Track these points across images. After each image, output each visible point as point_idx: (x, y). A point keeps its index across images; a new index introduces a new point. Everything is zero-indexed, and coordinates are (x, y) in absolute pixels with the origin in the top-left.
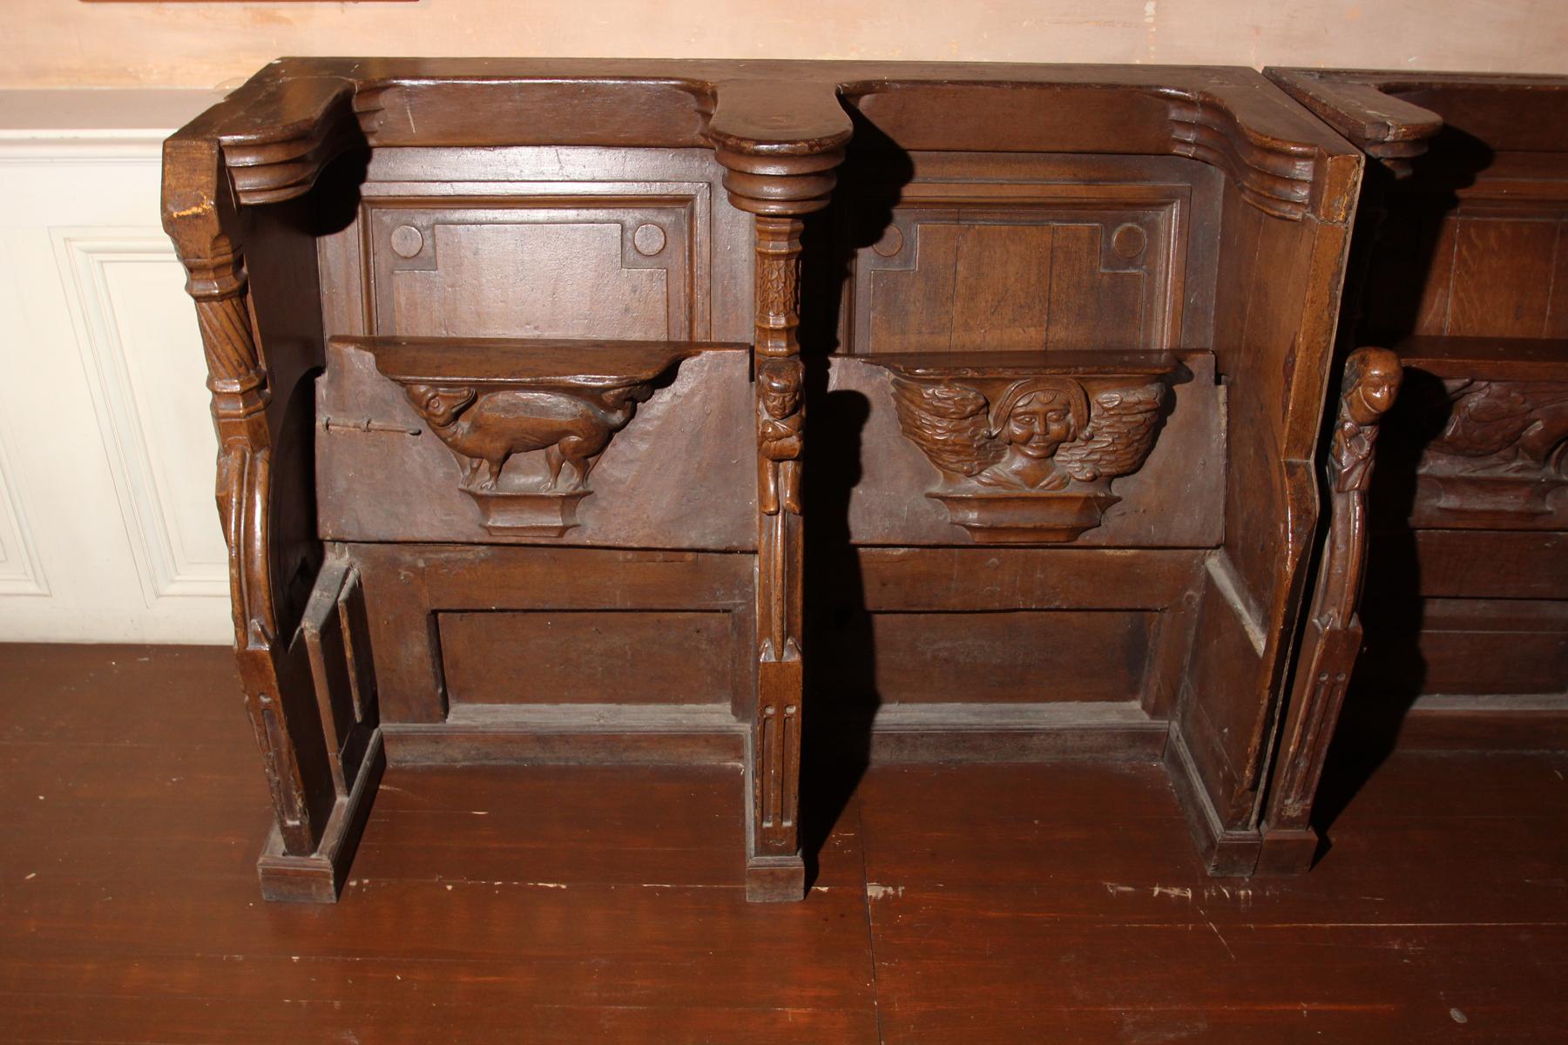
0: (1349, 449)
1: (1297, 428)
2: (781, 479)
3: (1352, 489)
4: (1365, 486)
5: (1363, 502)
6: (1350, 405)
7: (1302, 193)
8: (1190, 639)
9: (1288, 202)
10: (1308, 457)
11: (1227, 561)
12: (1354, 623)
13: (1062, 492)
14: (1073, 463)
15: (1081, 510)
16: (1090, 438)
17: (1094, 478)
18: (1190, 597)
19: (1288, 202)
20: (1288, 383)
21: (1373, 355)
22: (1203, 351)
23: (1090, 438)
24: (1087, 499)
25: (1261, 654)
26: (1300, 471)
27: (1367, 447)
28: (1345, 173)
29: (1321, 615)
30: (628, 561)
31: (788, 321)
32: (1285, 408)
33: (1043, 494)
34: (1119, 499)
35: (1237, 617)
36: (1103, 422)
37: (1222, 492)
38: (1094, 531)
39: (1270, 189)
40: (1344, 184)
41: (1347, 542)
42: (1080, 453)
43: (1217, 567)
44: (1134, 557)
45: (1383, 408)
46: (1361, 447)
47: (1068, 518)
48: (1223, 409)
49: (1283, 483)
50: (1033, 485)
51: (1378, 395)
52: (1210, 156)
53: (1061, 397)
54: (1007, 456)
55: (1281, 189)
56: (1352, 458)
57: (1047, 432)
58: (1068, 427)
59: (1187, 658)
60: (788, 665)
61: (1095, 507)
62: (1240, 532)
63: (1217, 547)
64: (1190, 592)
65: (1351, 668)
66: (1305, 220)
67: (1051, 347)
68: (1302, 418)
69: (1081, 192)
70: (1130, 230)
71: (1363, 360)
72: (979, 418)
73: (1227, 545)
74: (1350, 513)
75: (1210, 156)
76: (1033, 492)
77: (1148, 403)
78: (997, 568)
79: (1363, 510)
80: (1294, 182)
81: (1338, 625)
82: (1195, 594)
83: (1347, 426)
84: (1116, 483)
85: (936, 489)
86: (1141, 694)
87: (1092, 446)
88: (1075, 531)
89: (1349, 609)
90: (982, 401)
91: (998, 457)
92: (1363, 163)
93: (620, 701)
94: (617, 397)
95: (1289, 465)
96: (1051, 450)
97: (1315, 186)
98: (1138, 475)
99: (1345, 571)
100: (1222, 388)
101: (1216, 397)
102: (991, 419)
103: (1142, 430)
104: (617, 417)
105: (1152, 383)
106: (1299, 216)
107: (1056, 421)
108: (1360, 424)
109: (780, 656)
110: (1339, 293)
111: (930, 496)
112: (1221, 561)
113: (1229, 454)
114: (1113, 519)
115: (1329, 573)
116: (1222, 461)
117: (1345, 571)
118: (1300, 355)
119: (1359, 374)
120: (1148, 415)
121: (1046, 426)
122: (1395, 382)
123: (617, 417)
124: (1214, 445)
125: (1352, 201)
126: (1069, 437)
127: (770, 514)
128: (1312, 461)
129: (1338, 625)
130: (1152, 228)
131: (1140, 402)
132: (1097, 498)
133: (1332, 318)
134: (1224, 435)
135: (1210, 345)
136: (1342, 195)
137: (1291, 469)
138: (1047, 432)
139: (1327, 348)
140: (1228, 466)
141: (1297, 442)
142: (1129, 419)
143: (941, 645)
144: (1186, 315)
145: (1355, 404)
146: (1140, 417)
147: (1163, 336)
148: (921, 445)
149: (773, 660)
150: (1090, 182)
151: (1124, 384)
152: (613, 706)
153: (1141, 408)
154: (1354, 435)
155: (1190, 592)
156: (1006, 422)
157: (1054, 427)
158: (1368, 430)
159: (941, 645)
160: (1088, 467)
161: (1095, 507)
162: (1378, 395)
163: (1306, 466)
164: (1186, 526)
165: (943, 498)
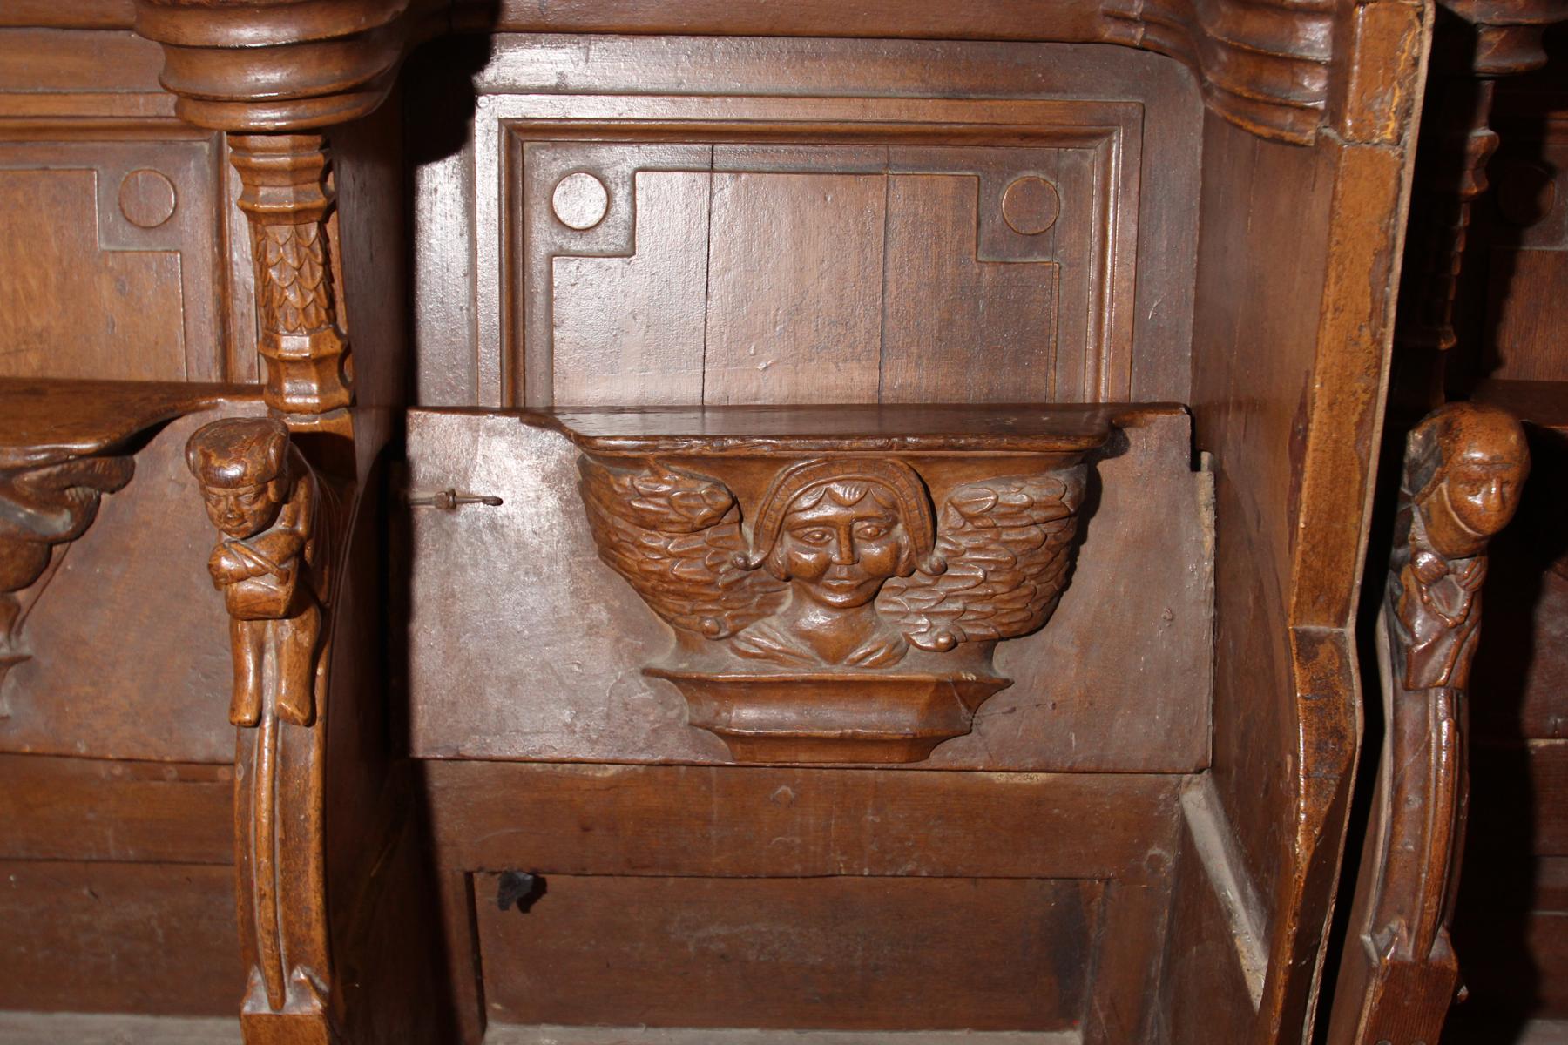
0: (1426, 604)
1: (1317, 564)
2: (270, 657)
3: (1432, 684)
4: (1459, 678)
5: (1454, 711)
6: (1427, 519)
7: (1315, 85)
8: (1161, 932)
9: (1286, 106)
10: (1341, 620)
11: (1216, 800)
12: (1440, 950)
13: (891, 673)
14: (918, 624)
15: (930, 705)
16: (940, 571)
17: (953, 645)
18: (1157, 860)
19: (1286, 106)
20: (1298, 473)
21: (1467, 419)
22: (1169, 407)
23: (940, 571)
24: (940, 685)
25: (1257, 1002)
26: (1324, 651)
27: (1462, 601)
28: (1391, 38)
29: (1377, 928)
30: (119, 779)
31: (315, 344)
32: (1293, 523)
33: (853, 674)
34: (1007, 683)
35: (1223, 916)
36: (964, 542)
37: (1207, 673)
38: (961, 741)
39: (1253, 83)
40: (1390, 62)
41: (1424, 791)
42: (927, 601)
43: (1199, 808)
44: (1046, 786)
45: (1489, 528)
46: (1450, 601)
47: (904, 719)
48: (1208, 517)
49: (1291, 675)
50: (835, 659)
51: (1478, 501)
52: (1167, 42)
53: (880, 493)
54: (788, 601)
55: (1272, 78)
56: (1436, 621)
57: (854, 558)
58: (897, 550)
59: (1157, 965)
60: (297, 1021)
61: (958, 700)
62: (1235, 751)
63: (1199, 771)
64: (1155, 851)
65: (1437, 1031)
66: (1322, 142)
67: (889, 397)
68: (1328, 546)
69: (932, 112)
70: (1031, 182)
71: (1448, 429)
72: (724, 532)
73: (1217, 768)
74: (1430, 729)
75: (1167, 42)
76: (837, 672)
77: (1045, 506)
78: (792, 803)
79: (1456, 728)
80: (1296, 64)
81: (1408, 953)
82: (1164, 854)
83: (1425, 559)
84: (1002, 653)
85: (660, 661)
86: (1083, 1020)
87: (943, 588)
88: (919, 746)
89: (1429, 920)
90: (723, 500)
91: (768, 605)
92: (1430, 19)
93: (158, 1010)
94: (40, 484)
95: (1302, 637)
96: (868, 589)
97: (1338, 72)
98: (1043, 636)
99: (1421, 849)
100: (1205, 478)
101: (1193, 493)
102: (748, 531)
103: (1042, 557)
104: (61, 522)
105: (1058, 467)
106: (1309, 136)
107: (872, 538)
108: (1445, 556)
109: (278, 1002)
110: (1393, 292)
111: (648, 672)
112: (1208, 797)
113: (1220, 598)
114: (995, 720)
115: (1390, 850)
116: (1207, 613)
117: (1421, 849)
118: (1317, 416)
119: (1442, 457)
120: (1051, 529)
121: (853, 548)
122: (1513, 474)
123: (61, 522)
124: (1190, 584)
125: (1409, 98)
126: (899, 567)
127: (242, 725)
128: (1350, 630)
129: (1408, 953)
130: (1075, 181)
131: (1031, 505)
132: (958, 683)
133: (1380, 344)
134: (1208, 565)
135: (1185, 397)
136: (1388, 84)
137: (1308, 645)
138: (854, 558)
139: (1370, 405)
140: (1217, 623)
141: (1319, 592)
142: (1014, 535)
143: (714, 930)
144: (1140, 340)
145: (1435, 514)
146: (1034, 532)
147: (1099, 382)
148: (629, 580)
149: (266, 1009)
150: (953, 95)
151: (1003, 469)
152: (146, 1020)
153: (1037, 515)
154: (1436, 578)
155: (1155, 851)
156: (776, 539)
157: (874, 551)
158: (1464, 566)
159: (714, 930)
160: (942, 623)
161: (958, 700)
162: (1478, 501)
163: (1338, 641)
164: (1137, 733)
165: (674, 679)
